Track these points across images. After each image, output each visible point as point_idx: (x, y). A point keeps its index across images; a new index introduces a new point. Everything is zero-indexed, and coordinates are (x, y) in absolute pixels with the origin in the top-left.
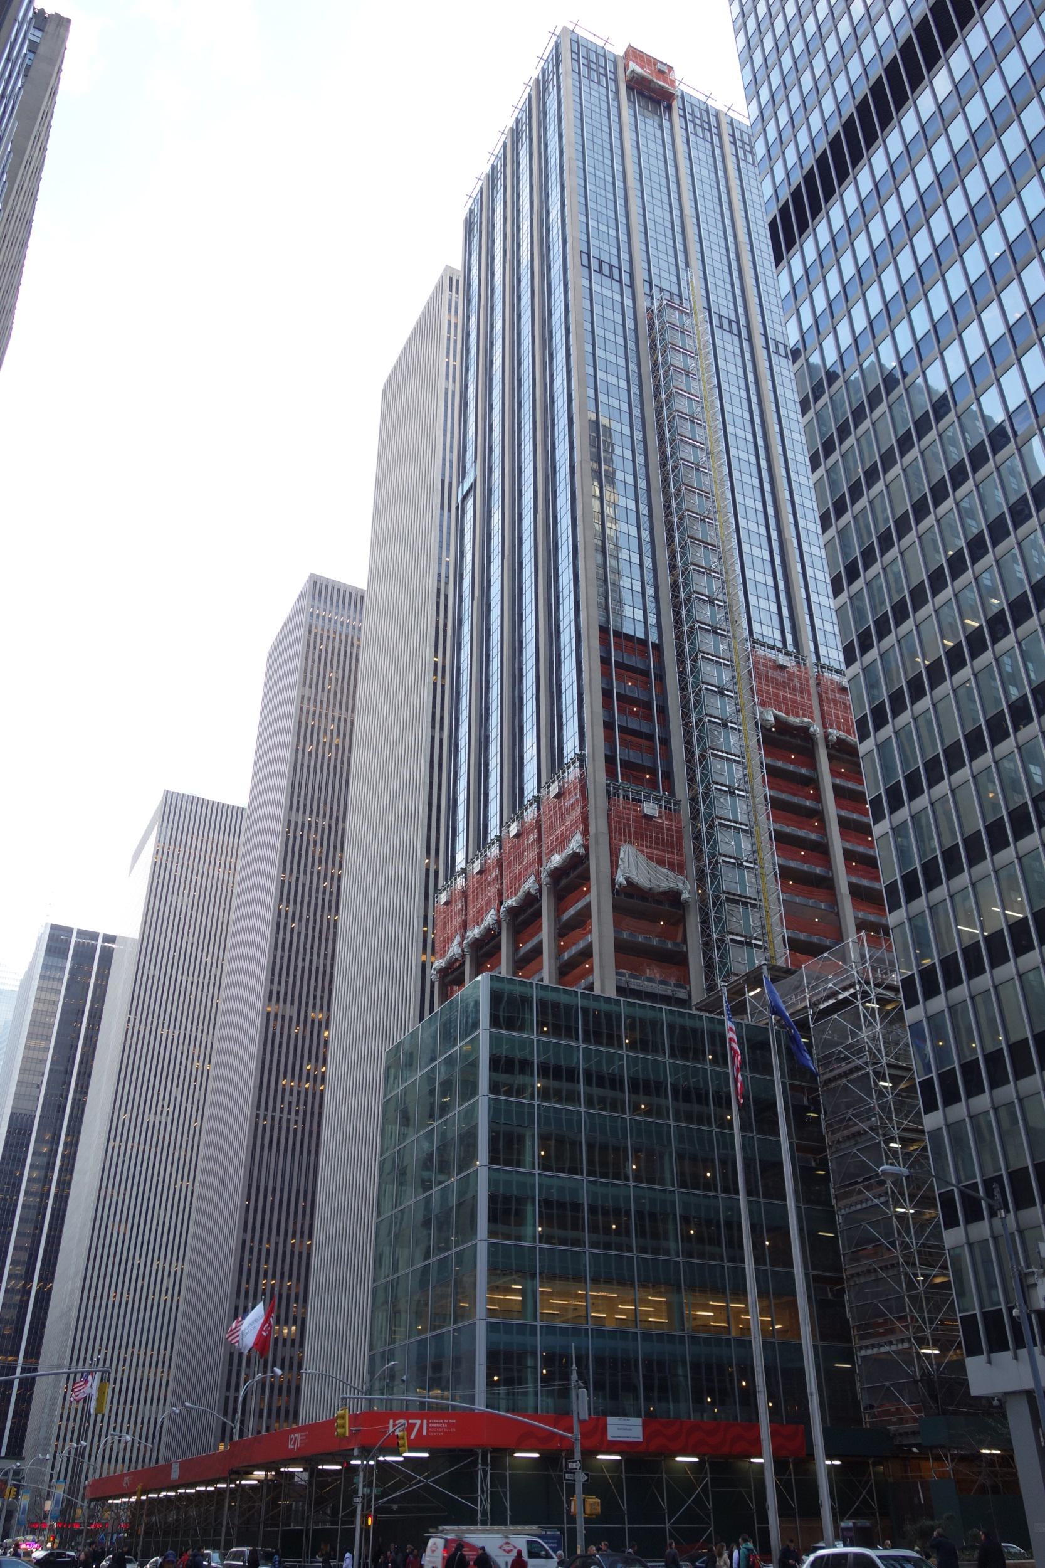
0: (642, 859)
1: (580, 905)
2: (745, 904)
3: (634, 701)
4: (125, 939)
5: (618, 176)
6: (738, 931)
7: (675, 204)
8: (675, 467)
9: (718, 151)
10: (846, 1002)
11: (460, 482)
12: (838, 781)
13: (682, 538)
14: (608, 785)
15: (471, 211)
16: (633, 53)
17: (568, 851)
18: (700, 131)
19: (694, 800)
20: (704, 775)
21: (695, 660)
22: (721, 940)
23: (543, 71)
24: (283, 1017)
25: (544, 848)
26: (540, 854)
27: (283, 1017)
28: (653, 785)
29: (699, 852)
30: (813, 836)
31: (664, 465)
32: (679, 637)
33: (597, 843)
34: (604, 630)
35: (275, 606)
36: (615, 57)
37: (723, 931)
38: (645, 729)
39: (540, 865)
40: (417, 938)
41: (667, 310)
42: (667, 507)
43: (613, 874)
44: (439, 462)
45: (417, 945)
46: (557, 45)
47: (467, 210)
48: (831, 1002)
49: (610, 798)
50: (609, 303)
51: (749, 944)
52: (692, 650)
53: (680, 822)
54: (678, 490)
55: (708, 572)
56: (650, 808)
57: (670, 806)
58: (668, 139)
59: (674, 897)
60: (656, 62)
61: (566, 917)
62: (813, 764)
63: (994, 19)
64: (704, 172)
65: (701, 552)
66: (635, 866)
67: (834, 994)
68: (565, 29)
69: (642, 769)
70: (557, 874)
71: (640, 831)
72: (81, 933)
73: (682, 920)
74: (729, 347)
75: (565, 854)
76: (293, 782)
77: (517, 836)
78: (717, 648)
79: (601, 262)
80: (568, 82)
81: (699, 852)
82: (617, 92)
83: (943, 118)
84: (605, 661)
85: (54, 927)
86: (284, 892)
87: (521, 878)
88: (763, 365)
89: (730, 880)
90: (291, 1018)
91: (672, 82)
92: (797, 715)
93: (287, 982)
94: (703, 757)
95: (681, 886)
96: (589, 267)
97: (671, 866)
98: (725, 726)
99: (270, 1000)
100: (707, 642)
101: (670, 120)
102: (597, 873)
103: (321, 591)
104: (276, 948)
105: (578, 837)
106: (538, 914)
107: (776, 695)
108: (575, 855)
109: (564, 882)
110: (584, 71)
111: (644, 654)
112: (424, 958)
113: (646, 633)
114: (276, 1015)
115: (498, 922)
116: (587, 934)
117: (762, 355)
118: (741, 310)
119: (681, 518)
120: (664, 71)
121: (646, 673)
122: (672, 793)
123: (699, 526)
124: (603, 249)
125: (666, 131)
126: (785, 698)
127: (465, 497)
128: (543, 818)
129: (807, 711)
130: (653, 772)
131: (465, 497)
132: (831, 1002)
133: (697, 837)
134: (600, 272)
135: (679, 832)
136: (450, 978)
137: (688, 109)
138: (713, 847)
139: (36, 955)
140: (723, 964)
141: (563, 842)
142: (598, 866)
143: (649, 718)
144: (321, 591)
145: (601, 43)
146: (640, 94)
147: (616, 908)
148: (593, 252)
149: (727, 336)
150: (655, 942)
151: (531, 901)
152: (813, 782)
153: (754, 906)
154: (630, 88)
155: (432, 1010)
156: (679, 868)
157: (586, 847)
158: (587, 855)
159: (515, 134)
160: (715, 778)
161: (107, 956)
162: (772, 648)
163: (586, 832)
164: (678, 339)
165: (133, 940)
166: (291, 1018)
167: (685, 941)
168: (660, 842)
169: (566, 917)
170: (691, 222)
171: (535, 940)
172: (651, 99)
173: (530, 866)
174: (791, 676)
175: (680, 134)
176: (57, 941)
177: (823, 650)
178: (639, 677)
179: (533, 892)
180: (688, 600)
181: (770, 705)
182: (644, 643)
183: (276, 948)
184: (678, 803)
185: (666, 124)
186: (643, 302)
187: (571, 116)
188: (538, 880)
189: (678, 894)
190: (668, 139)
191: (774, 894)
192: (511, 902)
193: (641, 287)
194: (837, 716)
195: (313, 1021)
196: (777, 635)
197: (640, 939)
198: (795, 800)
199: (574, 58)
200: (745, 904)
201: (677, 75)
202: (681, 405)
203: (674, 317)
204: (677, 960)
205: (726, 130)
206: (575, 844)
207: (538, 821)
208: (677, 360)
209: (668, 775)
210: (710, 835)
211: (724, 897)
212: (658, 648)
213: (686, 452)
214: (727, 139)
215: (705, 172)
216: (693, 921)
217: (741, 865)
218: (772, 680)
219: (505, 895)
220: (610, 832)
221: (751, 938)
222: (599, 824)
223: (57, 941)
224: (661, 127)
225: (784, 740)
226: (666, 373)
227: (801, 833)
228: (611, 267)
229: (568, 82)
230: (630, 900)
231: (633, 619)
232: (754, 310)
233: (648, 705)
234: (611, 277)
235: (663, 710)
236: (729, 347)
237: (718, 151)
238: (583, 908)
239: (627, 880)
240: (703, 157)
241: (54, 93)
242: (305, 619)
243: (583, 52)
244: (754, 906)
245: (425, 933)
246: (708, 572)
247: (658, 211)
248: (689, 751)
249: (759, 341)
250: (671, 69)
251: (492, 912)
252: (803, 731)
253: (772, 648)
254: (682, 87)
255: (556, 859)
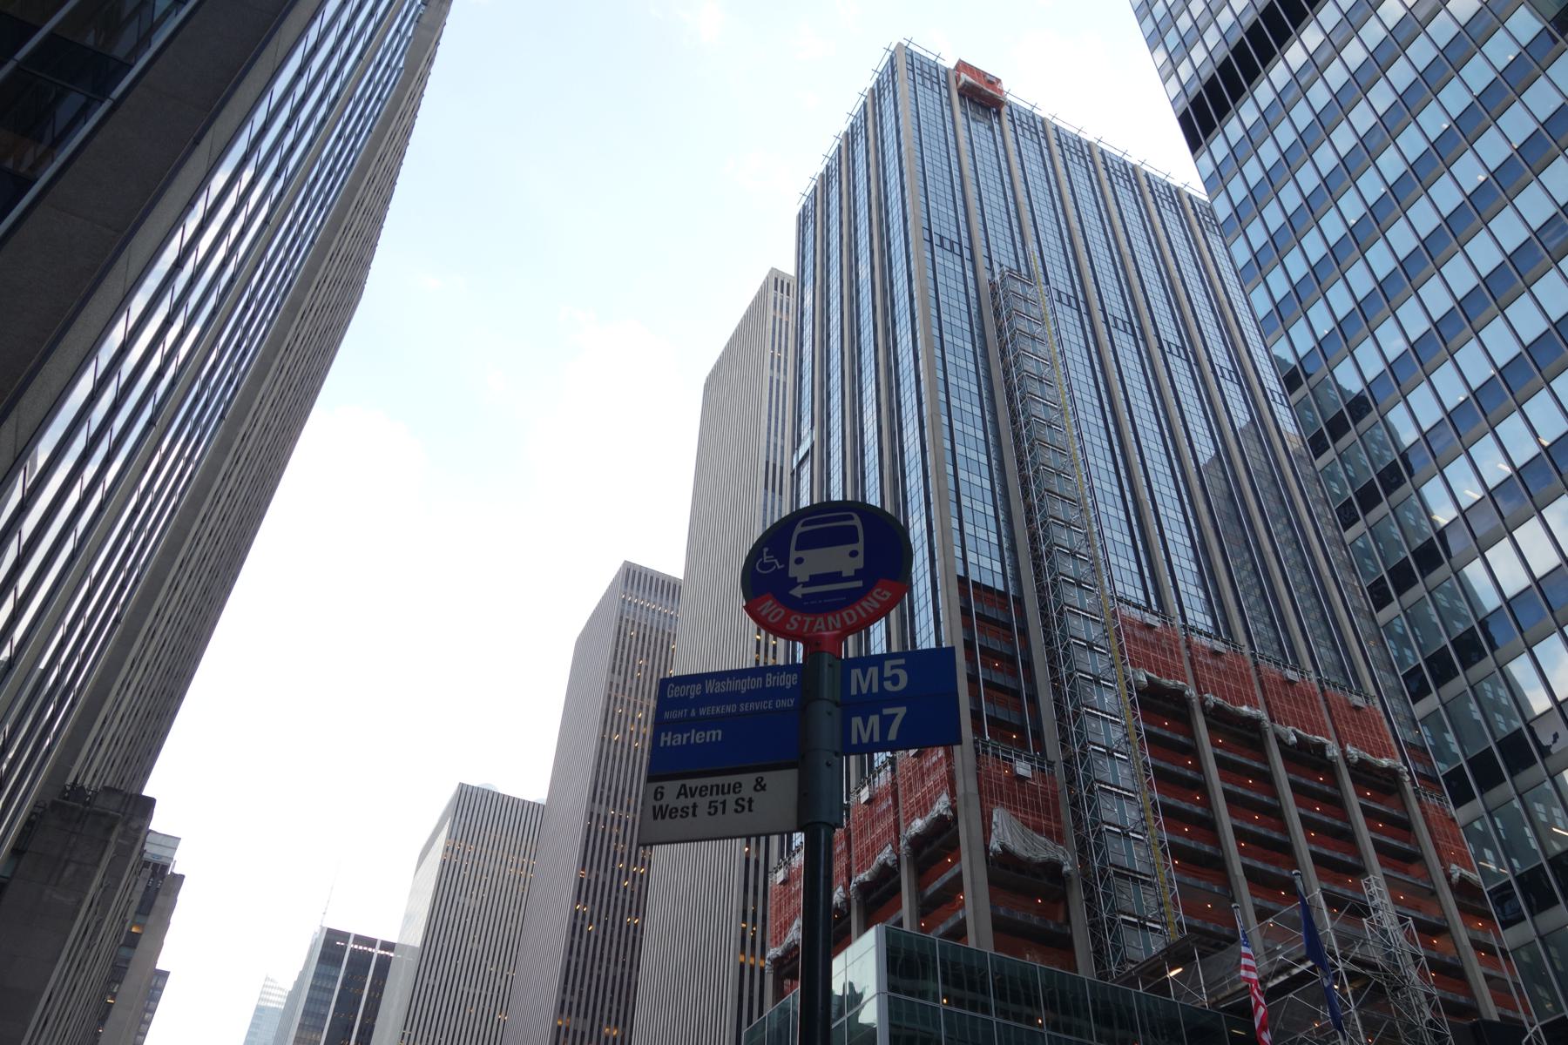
0: (1017, 824)
1: (947, 876)
2: (1135, 880)
3: (996, 655)
4: (404, 947)
5: (955, 166)
6: (1130, 910)
7: (1009, 193)
8: (1027, 424)
9: (1045, 152)
10: (1304, 977)
11: (795, 449)
12: (1218, 751)
13: (1039, 492)
14: (975, 742)
15: (804, 207)
16: (962, 66)
17: (933, 814)
18: (1027, 134)
19: (1068, 762)
20: (1080, 735)
21: (1061, 613)
22: (1112, 921)
23: (852, 126)
24: (575, 1032)
25: (901, 814)
26: (897, 822)
27: (575, 1032)
28: (1022, 743)
29: (1078, 821)
30: (1198, 810)
31: (1014, 422)
32: (1041, 589)
33: (966, 805)
34: (963, 581)
35: (590, 587)
36: (947, 72)
37: (1114, 911)
38: (1011, 685)
39: (897, 832)
40: (735, 934)
41: (1009, 281)
42: (1020, 462)
43: (987, 840)
44: (763, 444)
45: (735, 944)
46: (892, 59)
47: (800, 206)
48: (1282, 978)
49: (978, 756)
50: (952, 274)
51: (1144, 927)
52: (1057, 603)
53: (1055, 784)
54: (1032, 445)
55: (1068, 525)
56: (1023, 768)
57: (1042, 762)
58: (999, 139)
59: (1053, 868)
60: (985, 74)
61: (929, 891)
62: (1190, 731)
63: (1328, 15)
64: (1034, 168)
65: (1059, 506)
66: (1007, 831)
67: (1286, 968)
68: (900, 44)
69: (1011, 728)
70: (918, 842)
71: (1013, 793)
72: (359, 939)
73: (1063, 899)
74: (1069, 319)
75: (928, 818)
76: (598, 772)
77: (868, 802)
78: (1082, 601)
79: (942, 238)
80: (904, 87)
81: (1078, 821)
82: (949, 97)
83: (1317, 64)
84: (966, 612)
85: (330, 932)
86: (582, 891)
87: (873, 849)
88: (1104, 338)
89: (1117, 852)
90: (583, 1034)
91: (1001, 91)
92: (1169, 677)
93: (581, 993)
94: (1076, 715)
95: (1061, 857)
96: (931, 241)
97: (1049, 835)
98: (1098, 683)
99: (562, 1011)
100: (1073, 596)
101: (1000, 123)
102: (969, 838)
103: (634, 578)
104: (571, 953)
105: (944, 798)
106: (897, 889)
107: (1148, 656)
108: (941, 818)
109: (926, 851)
110: (919, 79)
111: (1005, 606)
112: (742, 958)
113: (1006, 585)
114: (567, 1029)
115: (847, 901)
116: (956, 910)
117: (1102, 329)
118: (1078, 288)
119: (1037, 471)
120: (993, 82)
121: (1009, 627)
122: (1044, 754)
123: (1055, 480)
124: (945, 226)
125: (997, 132)
126: (1156, 659)
127: (800, 464)
128: (900, 781)
129: (1180, 674)
130: (1021, 731)
131: (800, 464)
132: (1282, 978)
133: (1075, 803)
134: (942, 246)
135: (1055, 796)
136: (784, 971)
137: (1016, 115)
138: (1095, 814)
139: (302, 975)
140: (1117, 949)
141: (924, 807)
142: (968, 830)
143: (1015, 674)
144: (634, 578)
145: (933, 58)
146: (971, 100)
147: (992, 882)
148: (934, 229)
149: (1067, 310)
150: (1035, 920)
151: (887, 875)
152: (1192, 751)
153: (1150, 884)
154: (961, 95)
155: (750, 1022)
156: (1059, 838)
157: (953, 808)
158: (955, 819)
159: (825, 179)
160: (1091, 737)
161: (384, 965)
162: (1137, 607)
163: (953, 794)
164: (1022, 307)
165: (413, 948)
166: (583, 1034)
167: (1068, 921)
168: (1037, 808)
169: (929, 891)
170: (1025, 209)
171: (956, 869)
172: (981, 105)
173: (884, 834)
174: (1159, 637)
175: (1010, 136)
176: (332, 947)
177: (1188, 613)
178: (1001, 631)
179: (890, 863)
180: (1049, 553)
181: (1140, 665)
182: (1003, 595)
183: (571, 953)
184: (1051, 764)
185: (996, 127)
186: (985, 276)
187: (909, 114)
188: (896, 850)
189: (1059, 866)
190: (999, 139)
191: (1167, 872)
192: (864, 876)
193: (982, 263)
194: (1211, 681)
195: (607, 1038)
196: (1141, 595)
197: (1019, 916)
198: (1175, 769)
199: (906, 69)
200: (1135, 880)
201: (1005, 86)
202: (1030, 366)
203: (1018, 287)
204: (1062, 945)
205: (1052, 135)
206: (941, 805)
207: (894, 784)
208: (1022, 325)
209: (1038, 735)
210: (1091, 800)
211: (1111, 870)
212: (1019, 601)
213: (1037, 410)
214: (1054, 142)
215: (1035, 168)
216: (1077, 898)
217: (1127, 835)
218: (1142, 642)
219: (854, 869)
220: (980, 792)
221: (1146, 919)
222: (967, 784)
223: (332, 947)
224: (991, 128)
225: (1159, 704)
226: (1013, 336)
227: (1185, 806)
228: (952, 243)
229: (904, 87)
230: (1004, 867)
231: (987, 568)
232: (1091, 288)
233: (1012, 659)
234: (952, 250)
235: (1029, 665)
236: (1069, 319)
237: (1045, 152)
238: (951, 880)
239: (1002, 846)
240: (1032, 155)
241: (430, 62)
242: (617, 603)
243: (916, 64)
244: (1144, 882)
245: (744, 930)
246: (1068, 525)
247: (993, 198)
248: (1059, 708)
249: (1099, 317)
250: (999, 81)
251: (840, 889)
252: (1178, 694)
253: (1137, 607)
254: (1009, 97)
255: (918, 824)
